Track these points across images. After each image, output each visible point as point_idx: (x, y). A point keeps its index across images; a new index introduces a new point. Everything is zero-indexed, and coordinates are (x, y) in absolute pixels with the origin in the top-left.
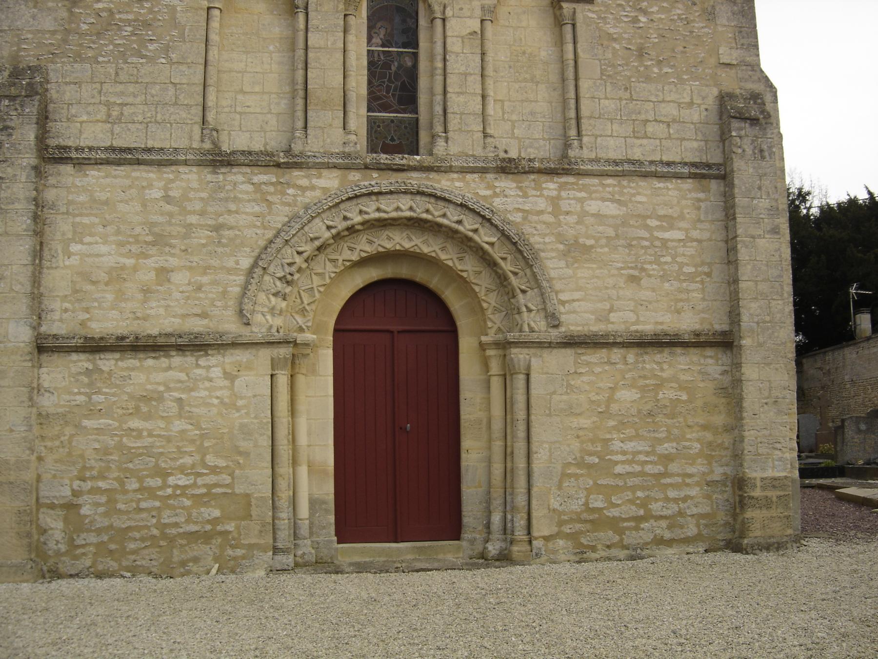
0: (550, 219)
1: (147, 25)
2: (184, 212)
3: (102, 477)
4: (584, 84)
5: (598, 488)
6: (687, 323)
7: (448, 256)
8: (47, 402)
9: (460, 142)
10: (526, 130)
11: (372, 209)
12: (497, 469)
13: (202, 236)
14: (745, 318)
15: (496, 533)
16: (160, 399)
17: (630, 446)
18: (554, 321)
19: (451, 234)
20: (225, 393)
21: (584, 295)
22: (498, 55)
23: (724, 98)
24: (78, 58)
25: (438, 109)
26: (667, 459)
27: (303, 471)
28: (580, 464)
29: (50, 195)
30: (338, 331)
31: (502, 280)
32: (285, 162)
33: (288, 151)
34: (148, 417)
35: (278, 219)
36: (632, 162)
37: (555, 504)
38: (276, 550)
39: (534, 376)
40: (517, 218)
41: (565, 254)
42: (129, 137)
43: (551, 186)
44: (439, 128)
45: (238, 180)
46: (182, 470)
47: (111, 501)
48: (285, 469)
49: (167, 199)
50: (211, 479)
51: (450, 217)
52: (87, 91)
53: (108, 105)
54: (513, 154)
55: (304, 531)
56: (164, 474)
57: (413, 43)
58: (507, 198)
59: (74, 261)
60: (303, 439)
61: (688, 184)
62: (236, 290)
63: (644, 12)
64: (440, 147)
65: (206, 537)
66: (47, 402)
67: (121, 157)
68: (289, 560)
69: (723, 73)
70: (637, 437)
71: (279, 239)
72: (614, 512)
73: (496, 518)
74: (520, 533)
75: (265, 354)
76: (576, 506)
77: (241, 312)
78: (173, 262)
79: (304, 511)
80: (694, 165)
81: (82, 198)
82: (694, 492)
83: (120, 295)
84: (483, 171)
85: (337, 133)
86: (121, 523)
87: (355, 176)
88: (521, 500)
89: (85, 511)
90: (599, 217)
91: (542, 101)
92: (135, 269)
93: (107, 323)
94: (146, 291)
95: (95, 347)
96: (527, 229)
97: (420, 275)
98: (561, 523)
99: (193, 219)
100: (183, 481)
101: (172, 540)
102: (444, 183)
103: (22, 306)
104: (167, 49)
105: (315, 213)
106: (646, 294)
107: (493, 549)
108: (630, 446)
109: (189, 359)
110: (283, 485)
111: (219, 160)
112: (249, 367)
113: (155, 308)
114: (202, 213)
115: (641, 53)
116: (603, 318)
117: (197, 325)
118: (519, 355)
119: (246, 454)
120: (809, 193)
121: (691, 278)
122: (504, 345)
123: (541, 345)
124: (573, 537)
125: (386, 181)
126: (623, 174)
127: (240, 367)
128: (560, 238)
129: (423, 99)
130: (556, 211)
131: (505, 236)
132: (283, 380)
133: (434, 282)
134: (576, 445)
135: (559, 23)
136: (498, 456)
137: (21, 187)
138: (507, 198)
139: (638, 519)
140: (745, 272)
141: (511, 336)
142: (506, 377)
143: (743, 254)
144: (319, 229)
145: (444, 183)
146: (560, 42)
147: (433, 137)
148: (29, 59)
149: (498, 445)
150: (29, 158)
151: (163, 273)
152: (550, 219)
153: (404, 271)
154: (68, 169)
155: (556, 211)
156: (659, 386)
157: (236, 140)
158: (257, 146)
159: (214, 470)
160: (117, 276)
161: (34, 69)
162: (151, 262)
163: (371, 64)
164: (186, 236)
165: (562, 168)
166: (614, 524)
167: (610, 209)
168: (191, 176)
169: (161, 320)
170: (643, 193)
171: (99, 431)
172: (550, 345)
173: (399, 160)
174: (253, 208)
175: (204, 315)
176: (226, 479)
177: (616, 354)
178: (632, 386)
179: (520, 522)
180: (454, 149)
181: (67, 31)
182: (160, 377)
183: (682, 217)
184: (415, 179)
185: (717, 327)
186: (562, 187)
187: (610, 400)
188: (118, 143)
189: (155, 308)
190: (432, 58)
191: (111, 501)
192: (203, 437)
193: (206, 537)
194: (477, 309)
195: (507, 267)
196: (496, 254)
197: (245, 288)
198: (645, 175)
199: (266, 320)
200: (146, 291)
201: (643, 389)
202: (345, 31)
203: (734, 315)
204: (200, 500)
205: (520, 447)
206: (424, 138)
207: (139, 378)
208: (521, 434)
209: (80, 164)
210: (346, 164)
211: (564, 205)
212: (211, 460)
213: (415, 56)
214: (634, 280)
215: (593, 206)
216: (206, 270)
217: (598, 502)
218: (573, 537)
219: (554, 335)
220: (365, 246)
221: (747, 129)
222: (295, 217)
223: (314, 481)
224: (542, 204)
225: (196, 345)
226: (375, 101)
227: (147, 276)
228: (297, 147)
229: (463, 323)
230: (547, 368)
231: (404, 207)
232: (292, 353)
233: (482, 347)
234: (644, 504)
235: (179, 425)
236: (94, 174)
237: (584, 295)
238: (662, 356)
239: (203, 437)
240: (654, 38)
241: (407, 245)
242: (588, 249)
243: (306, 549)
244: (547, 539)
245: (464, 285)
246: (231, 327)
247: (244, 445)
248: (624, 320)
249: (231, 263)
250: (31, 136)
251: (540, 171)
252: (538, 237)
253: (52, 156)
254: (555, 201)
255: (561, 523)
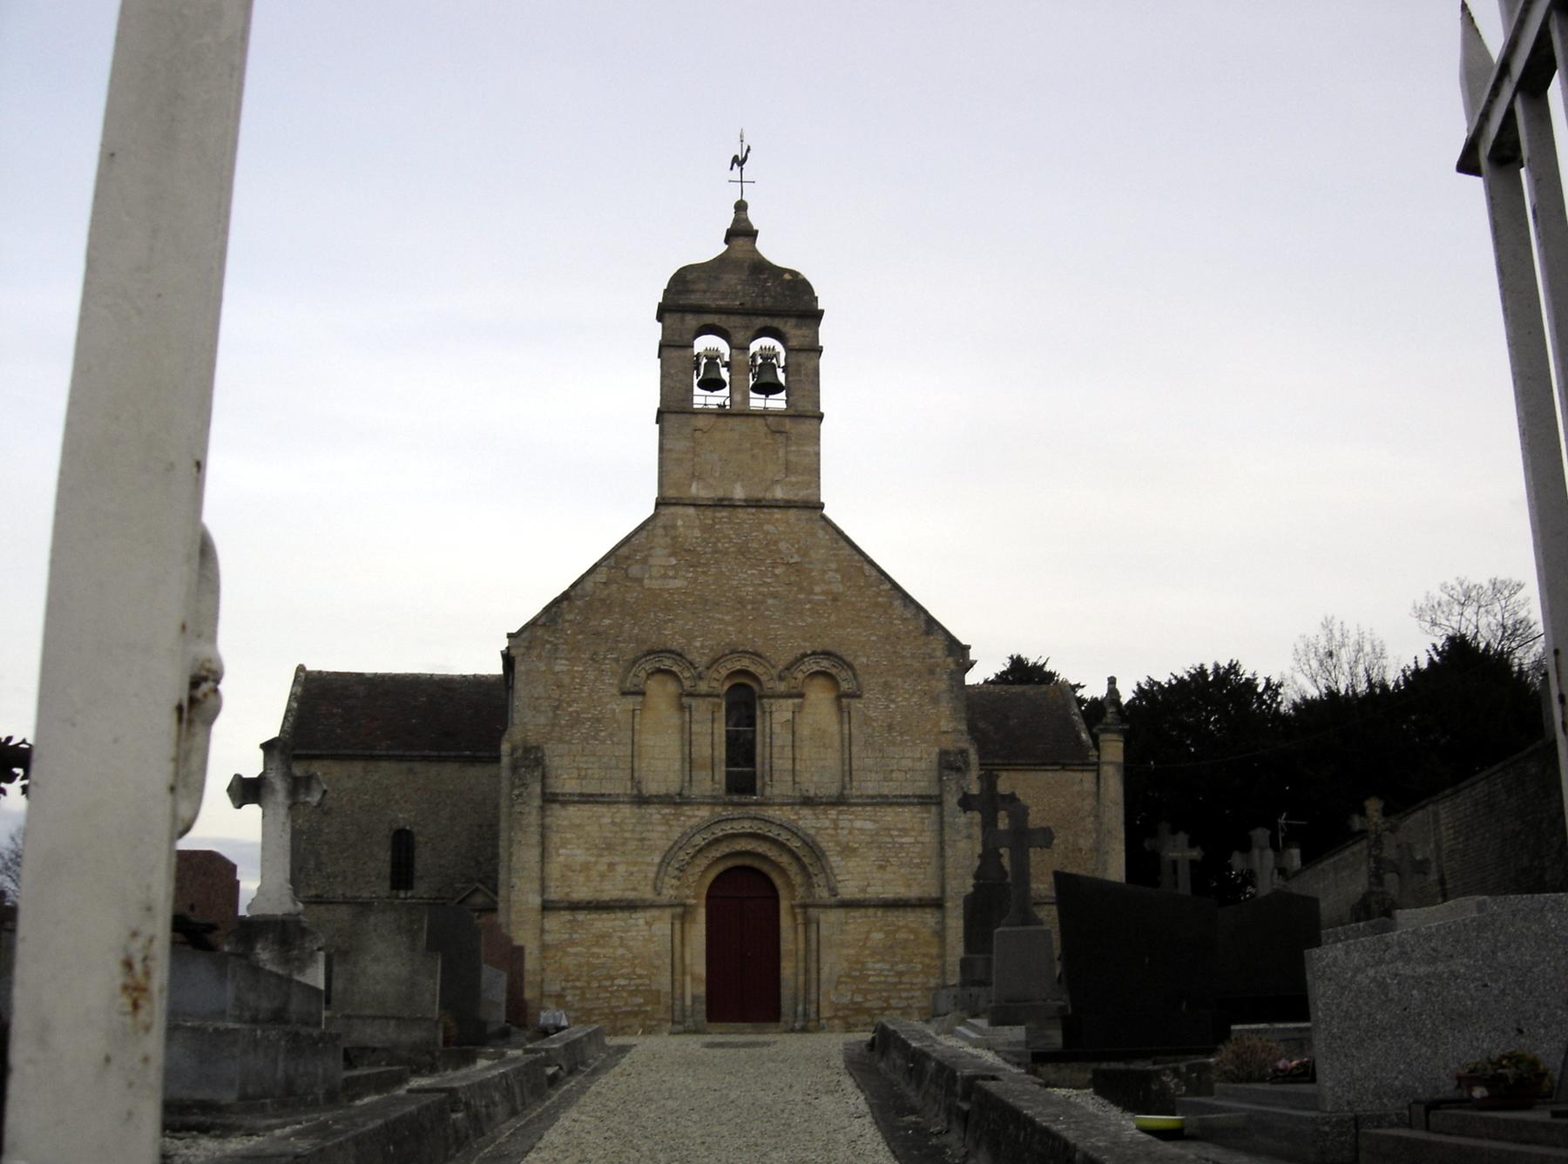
0: (831, 832)
1: (599, 721)
2: (623, 831)
3: (578, 979)
4: (854, 749)
5: (859, 991)
6: (914, 893)
7: (773, 853)
8: (548, 938)
9: (780, 787)
10: (820, 773)
11: (728, 828)
12: (801, 978)
13: (632, 845)
14: (948, 888)
15: (800, 1018)
16: (610, 936)
17: (878, 966)
18: (833, 892)
19: (774, 842)
20: (646, 933)
21: (852, 876)
22: (805, 731)
23: (943, 754)
24: (561, 740)
25: (767, 767)
26: (900, 974)
27: (688, 979)
28: (849, 976)
29: (548, 821)
30: (709, 897)
31: (803, 868)
32: (677, 801)
33: (680, 794)
34: (603, 947)
35: (676, 835)
36: (882, 796)
37: (833, 999)
38: (674, 1022)
39: (822, 925)
40: (812, 832)
41: (840, 853)
42: (592, 788)
43: (833, 813)
44: (767, 779)
45: (654, 813)
46: (622, 976)
47: (583, 993)
48: (678, 977)
49: (613, 823)
50: (638, 981)
51: (774, 832)
52: (566, 761)
53: (579, 769)
54: (812, 793)
55: (688, 1013)
56: (613, 978)
57: (752, 723)
58: (807, 820)
59: (561, 859)
60: (688, 960)
61: (917, 809)
62: (652, 875)
63: (893, 701)
64: (768, 791)
65: (636, 1014)
66: (548, 938)
67: (587, 799)
68: (680, 1028)
69: (943, 738)
70: (883, 960)
71: (676, 847)
72: (868, 1005)
73: (800, 1008)
74: (813, 1016)
75: (668, 913)
76: (845, 1000)
77: (655, 888)
78: (617, 859)
79: (688, 1002)
80: (921, 797)
81: (565, 823)
82: (918, 993)
83: (588, 879)
84: (792, 804)
85: (708, 784)
86: (588, 1005)
87: (719, 809)
88: (813, 996)
89: (569, 998)
90: (861, 830)
91: (832, 759)
92: (596, 863)
93: (581, 893)
94: (603, 876)
95: (574, 907)
96: (818, 839)
97: (756, 864)
98: (837, 1010)
99: (627, 835)
100: (623, 982)
101: (616, 1015)
102: (772, 813)
103: (536, 885)
104: (611, 735)
105: (700, 830)
106: (888, 876)
107: (798, 1025)
108: (878, 966)
109: (627, 914)
110: (677, 985)
111: (641, 800)
112: (660, 919)
113: (607, 886)
114: (633, 831)
115: (890, 728)
116: (863, 890)
117: (631, 895)
118: (813, 912)
119: (657, 968)
120: (1280, 685)
121: (918, 866)
122: (805, 906)
123: (825, 906)
124: (844, 1018)
125: (737, 812)
126: (877, 804)
127: (654, 919)
128: (838, 843)
129: (758, 759)
130: (836, 828)
131: (805, 843)
132: (678, 926)
133: (765, 868)
134: (845, 964)
135: (840, 709)
136: (801, 972)
137: (533, 818)
138: (807, 820)
139: (883, 1009)
140: (950, 862)
141: (808, 901)
142: (807, 923)
143: (949, 852)
144: (699, 840)
145: (772, 813)
146: (841, 722)
147: (764, 785)
148: (533, 740)
149: (801, 965)
150: (537, 802)
151: (611, 866)
152: (831, 832)
153: (747, 862)
154: (556, 806)
155: (836, 828)
156: (896, 931)
157: (652, 788)
158: (663, 791)
159: (640, 977)
160: (586, 867)
161: (538, 748)
162: (605, 860)
163: (728, 737)
164: (624, 844)
165: (840, 801)
166: (869, 1011)
167: (869, 825)
168: (626, 810)
169: (611, 892)
170: (889, 815)
171: (576, 954)
172: (831, 907)
173: (744, 799)
174: (661, 829)
175: (634, 889)
176: (647, 981)
177: (871, 911)
178: (881, 930)
179: (813, 1009)
180: (776, 792)
181: (553, 725)
182: (609, 924)
183: (913, 829)
184: (753, 811)
185: (934, 895)
186: (840, 813)
187: (867, 938)
188: (585, 791)
189: (607, 886)
190: (764, 736)
191: (583, 993)
192: (635, 958)
193: (636, 1014)
194: (790, 885)
195: (806, 860)
196: (800, 853)
197: (658, 873)
198: (891, 804)
199: (668, 893)
200: (603, 876)
201: (887, 933)
202: (713, 721)
203: (943, 888)
204: (632, 993)
205: (813, 966)
206: (759, 784)
207: (599, 924)
208: (814, 958)
209: (564, 804)
210: (714, 802)
211: (841, 824)
212: (639, 971)
213: (754, 732)
214: (881, 867)
215: (858, 824)
216: (635, 864)
217: (859, 999)
218: (844, 1018)
219: (833, 900)
220: (725, 849)
221: (954, 775)
222: (685, 834)
223: (695, 987)
224: (827, 823)
225: (630, 906)
226: (730, 761)
227: (603, 868)
228: (686, 792)
229: (783, 893)
230: (830, 920)
231: (747, 826)
232: (683, 913)
233: (793, 907)
234: (887, 1000)
235: (620, 951)
236: (571, 809)
237: (852, 876)
238: (900, 913)
239: (635, 958)
240: (899, 718)
241: (749, 848)
242: (855, 850)
243: (689, 1023)
244: (829, 1019)
245: (782, 871)
246: (649, 894)
247: (657, 962)
248: (877, 891)
249: (648, 859)
250: (538, 789)
251: (826, 804)
252: (825, 843)
253: (550, 799)
254: (835, 822)
255: (837, 1010)
